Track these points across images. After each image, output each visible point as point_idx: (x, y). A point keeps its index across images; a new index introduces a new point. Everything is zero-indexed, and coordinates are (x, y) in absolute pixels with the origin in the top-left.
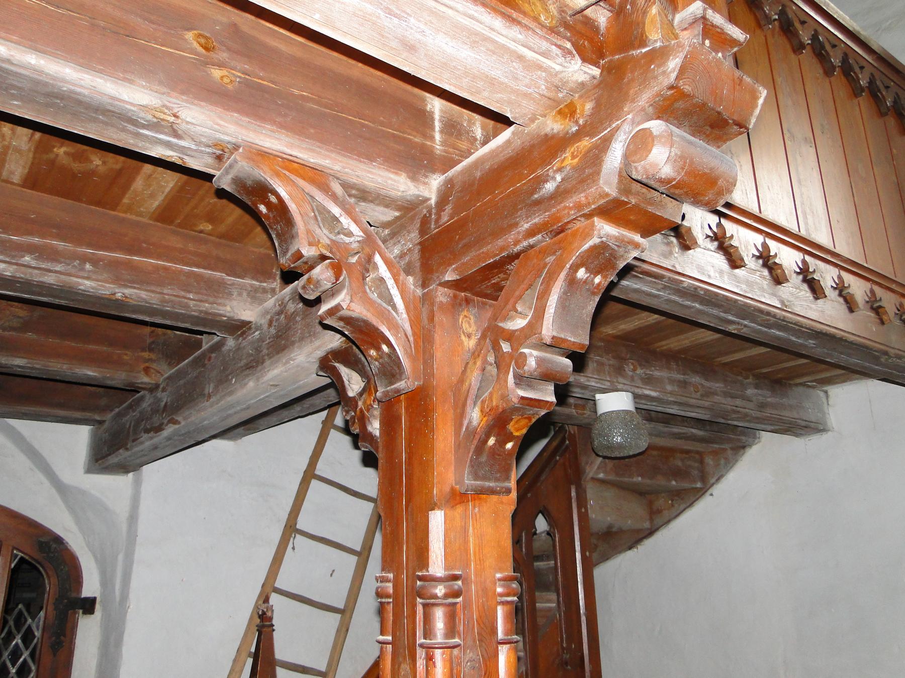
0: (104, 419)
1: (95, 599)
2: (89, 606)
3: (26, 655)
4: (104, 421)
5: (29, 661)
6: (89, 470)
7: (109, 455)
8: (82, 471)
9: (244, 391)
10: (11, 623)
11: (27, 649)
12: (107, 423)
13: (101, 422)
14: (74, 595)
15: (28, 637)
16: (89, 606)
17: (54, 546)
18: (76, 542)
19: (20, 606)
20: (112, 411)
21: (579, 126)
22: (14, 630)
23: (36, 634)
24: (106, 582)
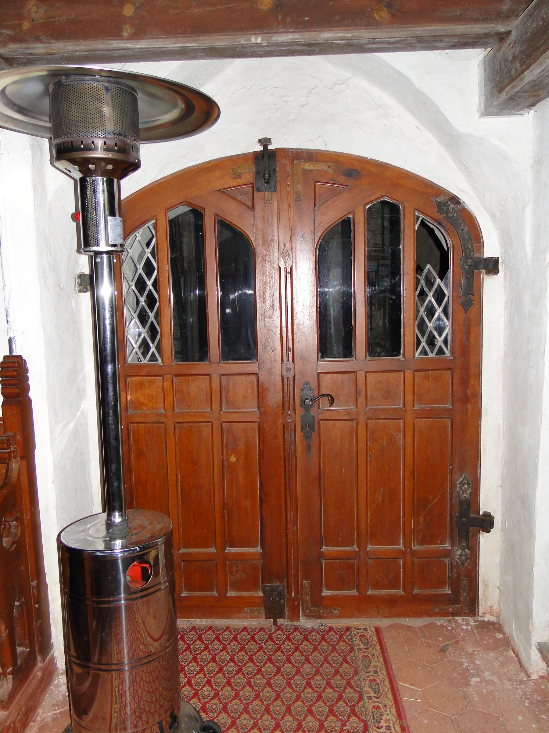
0: (509, 29)
1: (498, 258)
2: (492, 266)
3: (439, 311)
4: (509, 33)
5: (443, 316)
6: (489, 110)
7: (523, 72)
8: (477, 115)
9: (332, 317)
10: (423, 282)
11: (440, 306)
12: (514, 33)
13: (502, 37)
14: (477, 255)
15: (440, 296)
16: (492, 266)
17: (452, 206)
18: (472, 202)
19: (428, 266)
20: (517, 16)
21: (525, 699)
22: (426, 289)
23: (446, 292)
24: (506, 240)
